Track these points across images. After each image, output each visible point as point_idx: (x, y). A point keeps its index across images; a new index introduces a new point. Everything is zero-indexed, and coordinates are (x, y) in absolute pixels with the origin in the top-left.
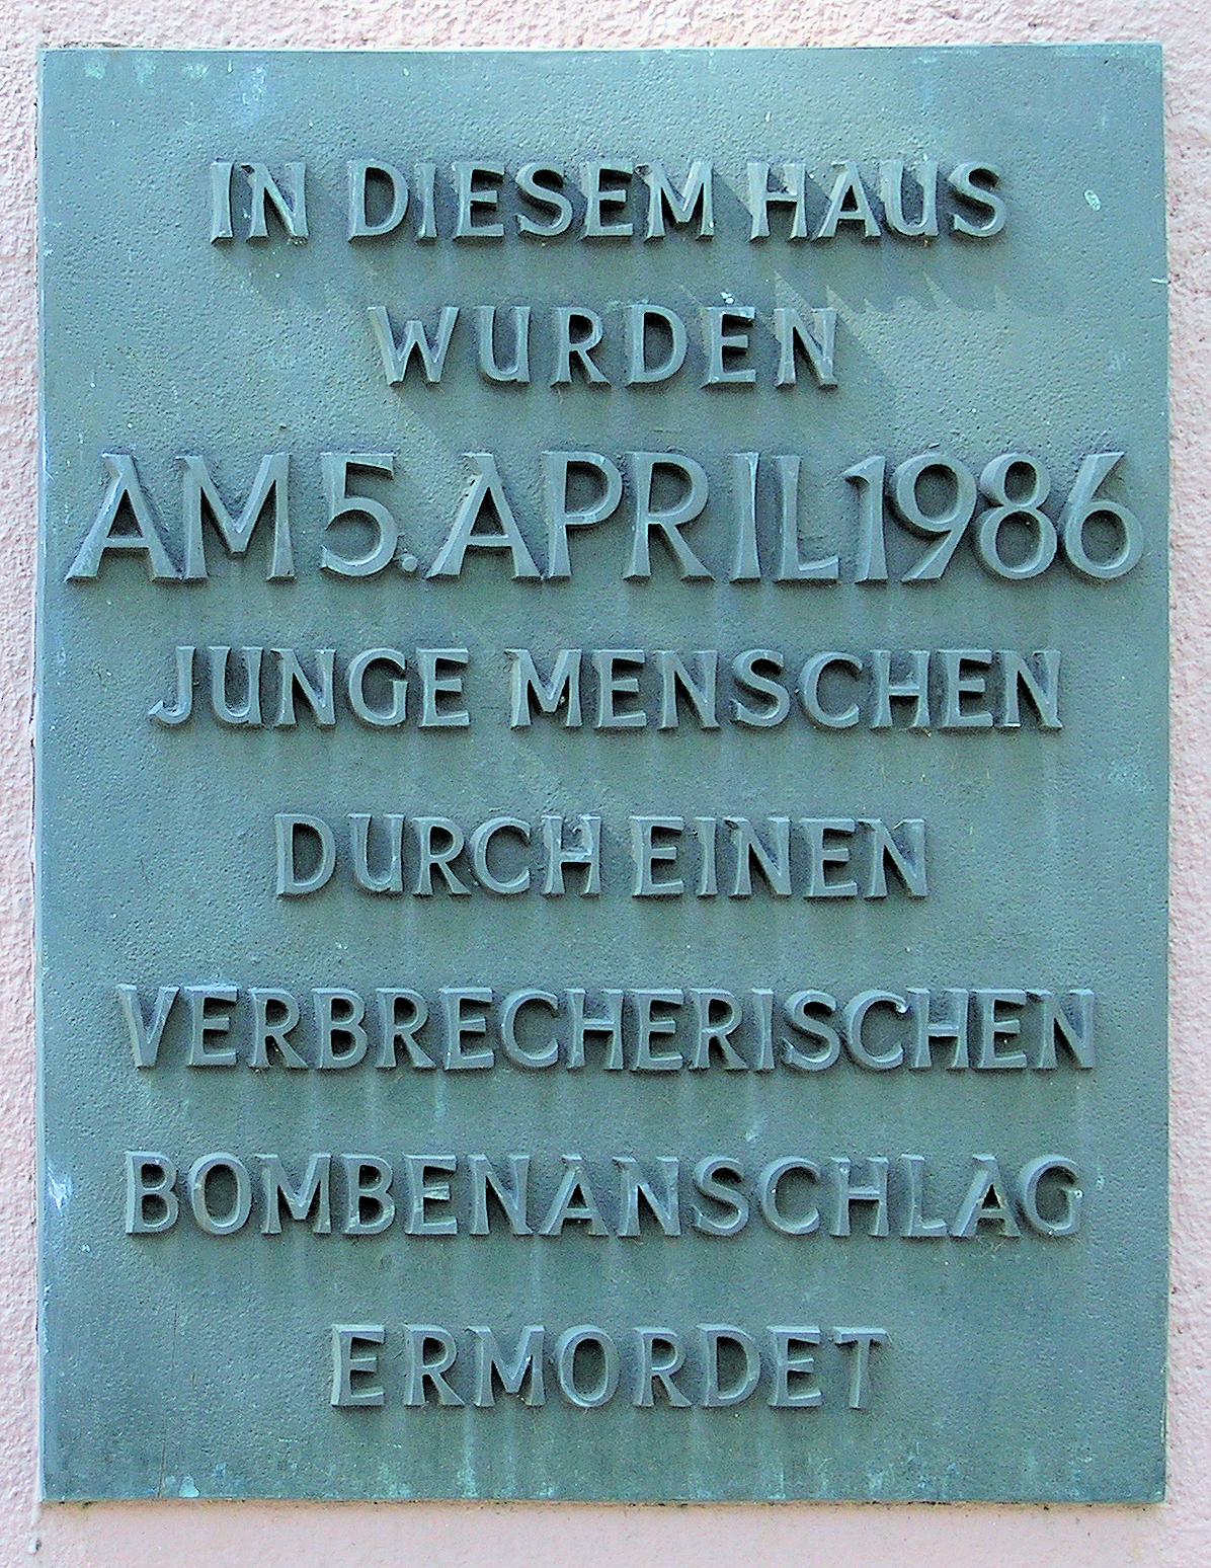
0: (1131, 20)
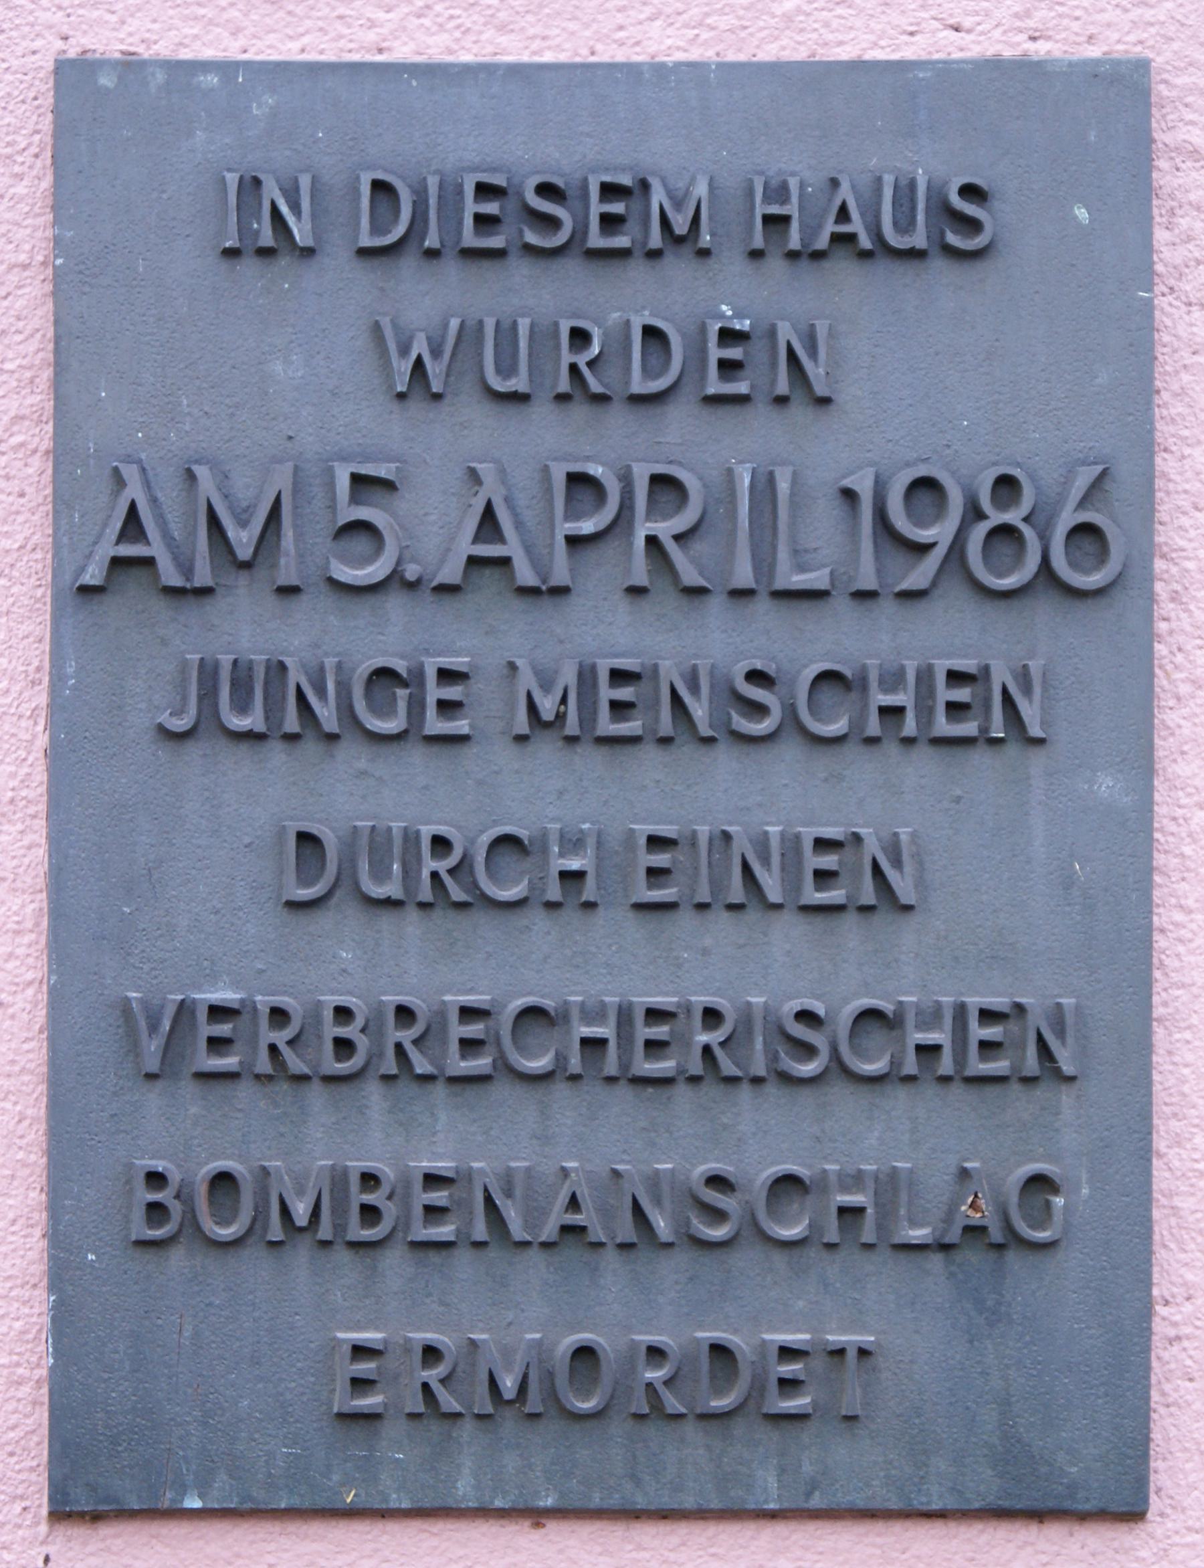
0: (1129, 33)
